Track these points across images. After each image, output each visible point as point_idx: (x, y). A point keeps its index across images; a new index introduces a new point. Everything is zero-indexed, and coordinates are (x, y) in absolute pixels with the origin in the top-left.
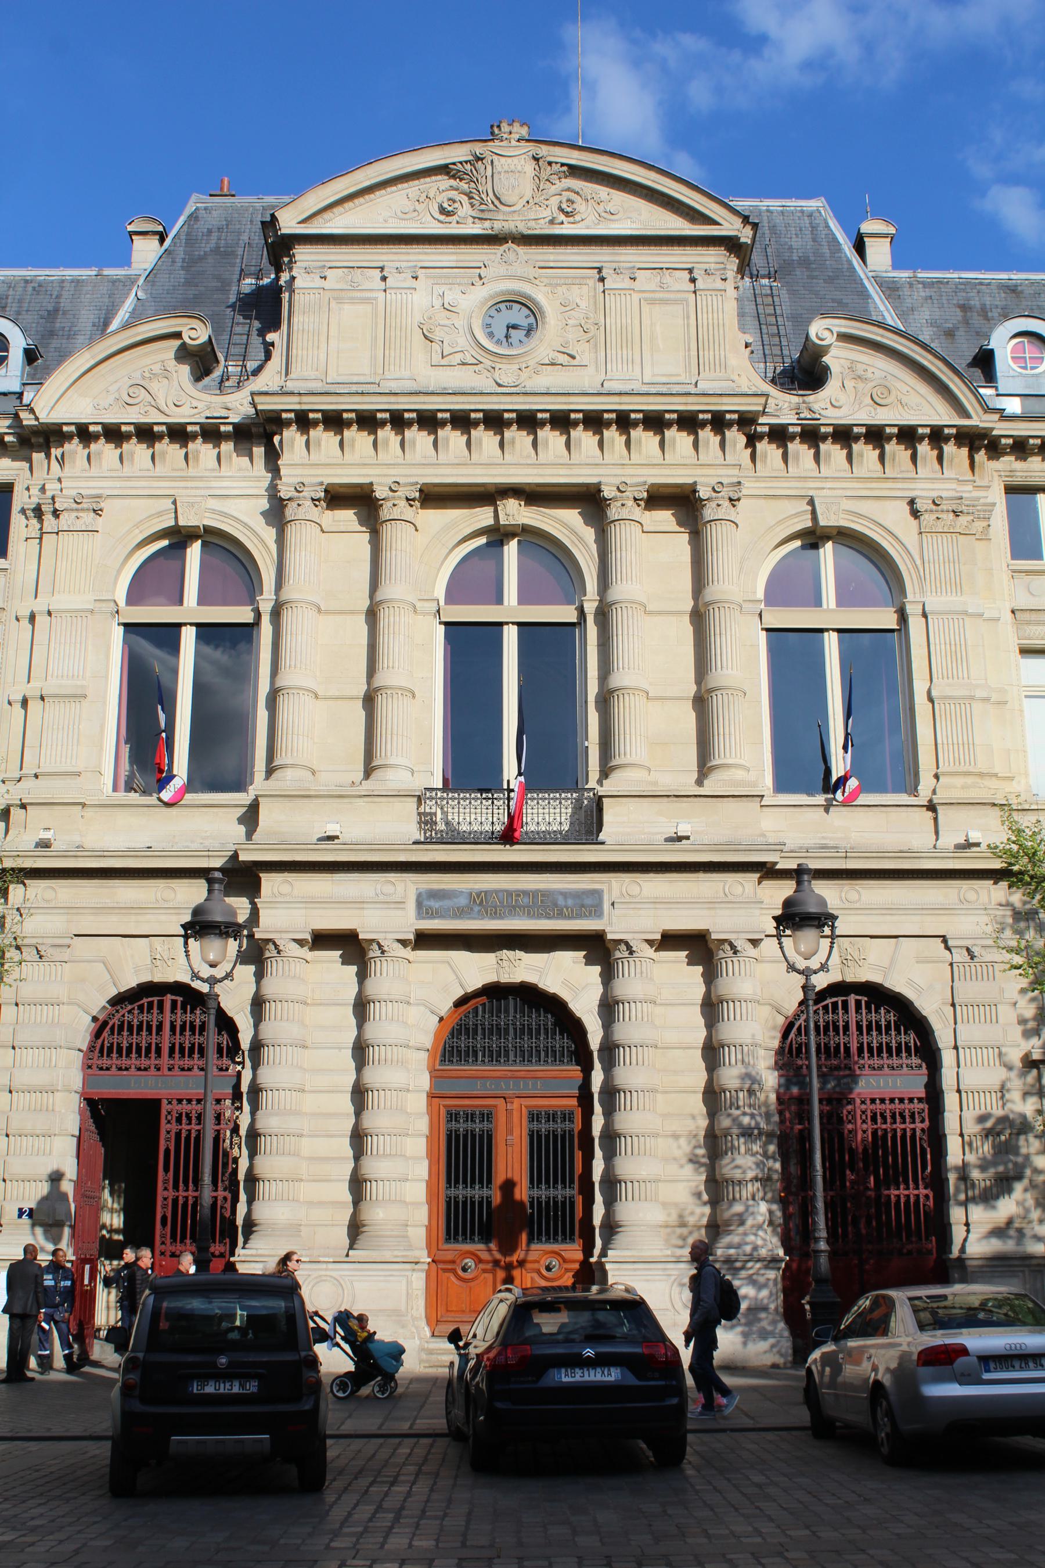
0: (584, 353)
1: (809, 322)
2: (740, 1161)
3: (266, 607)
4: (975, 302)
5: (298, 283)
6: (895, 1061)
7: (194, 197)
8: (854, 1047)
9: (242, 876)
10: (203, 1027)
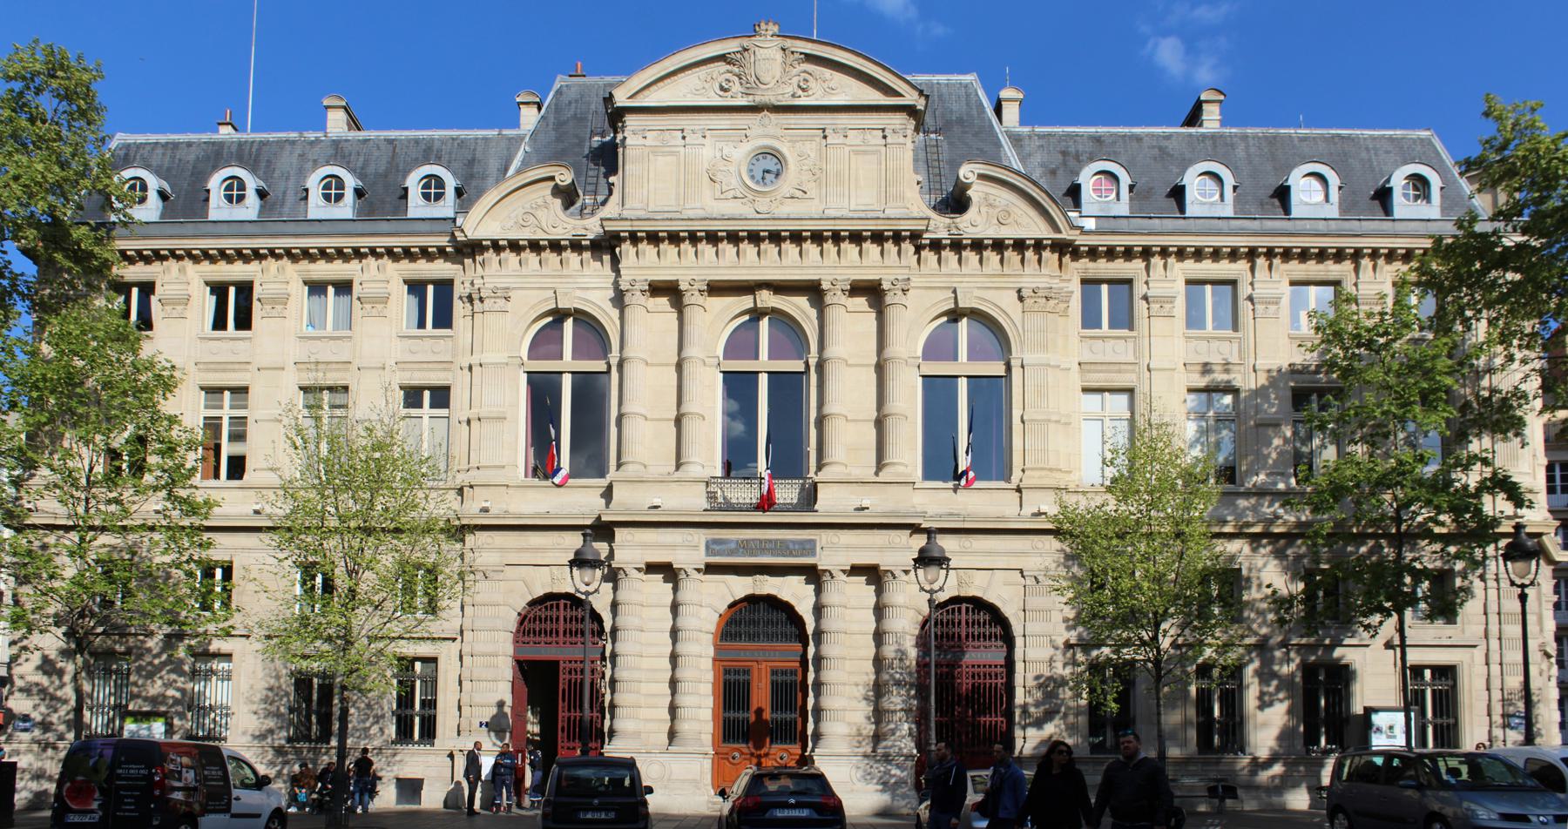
0: (811, 188)
1: (959, 165)
2: (893, 699)
3: (614, 362)
4: (1072, 149)
5: (628, 142)
6: (988, 643)
7: (559, 78)
8: (963, 635)
9: (603, 530)
10: (583, 619)
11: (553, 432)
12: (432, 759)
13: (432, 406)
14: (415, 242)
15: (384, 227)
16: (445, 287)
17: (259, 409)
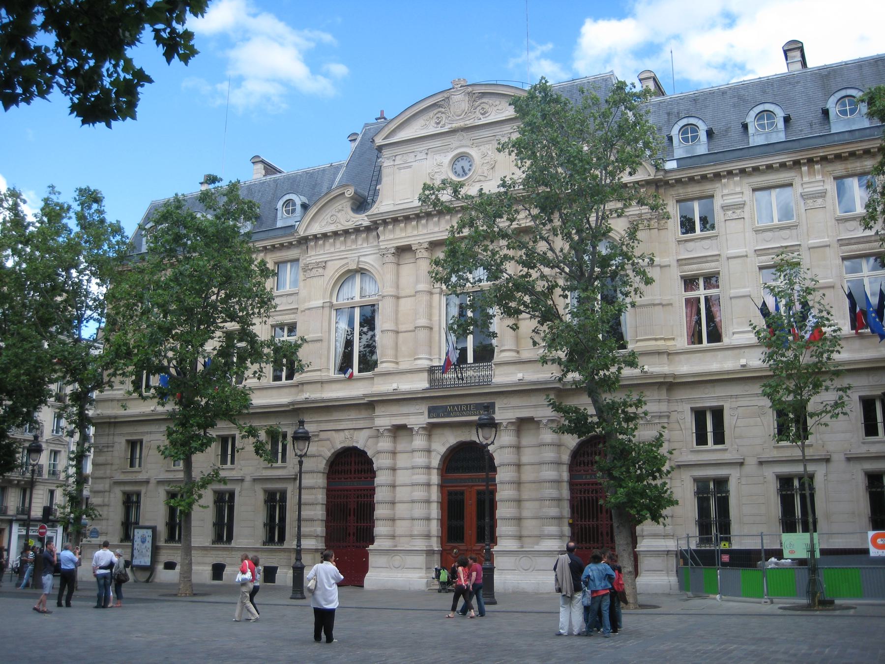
17: (727, 290)
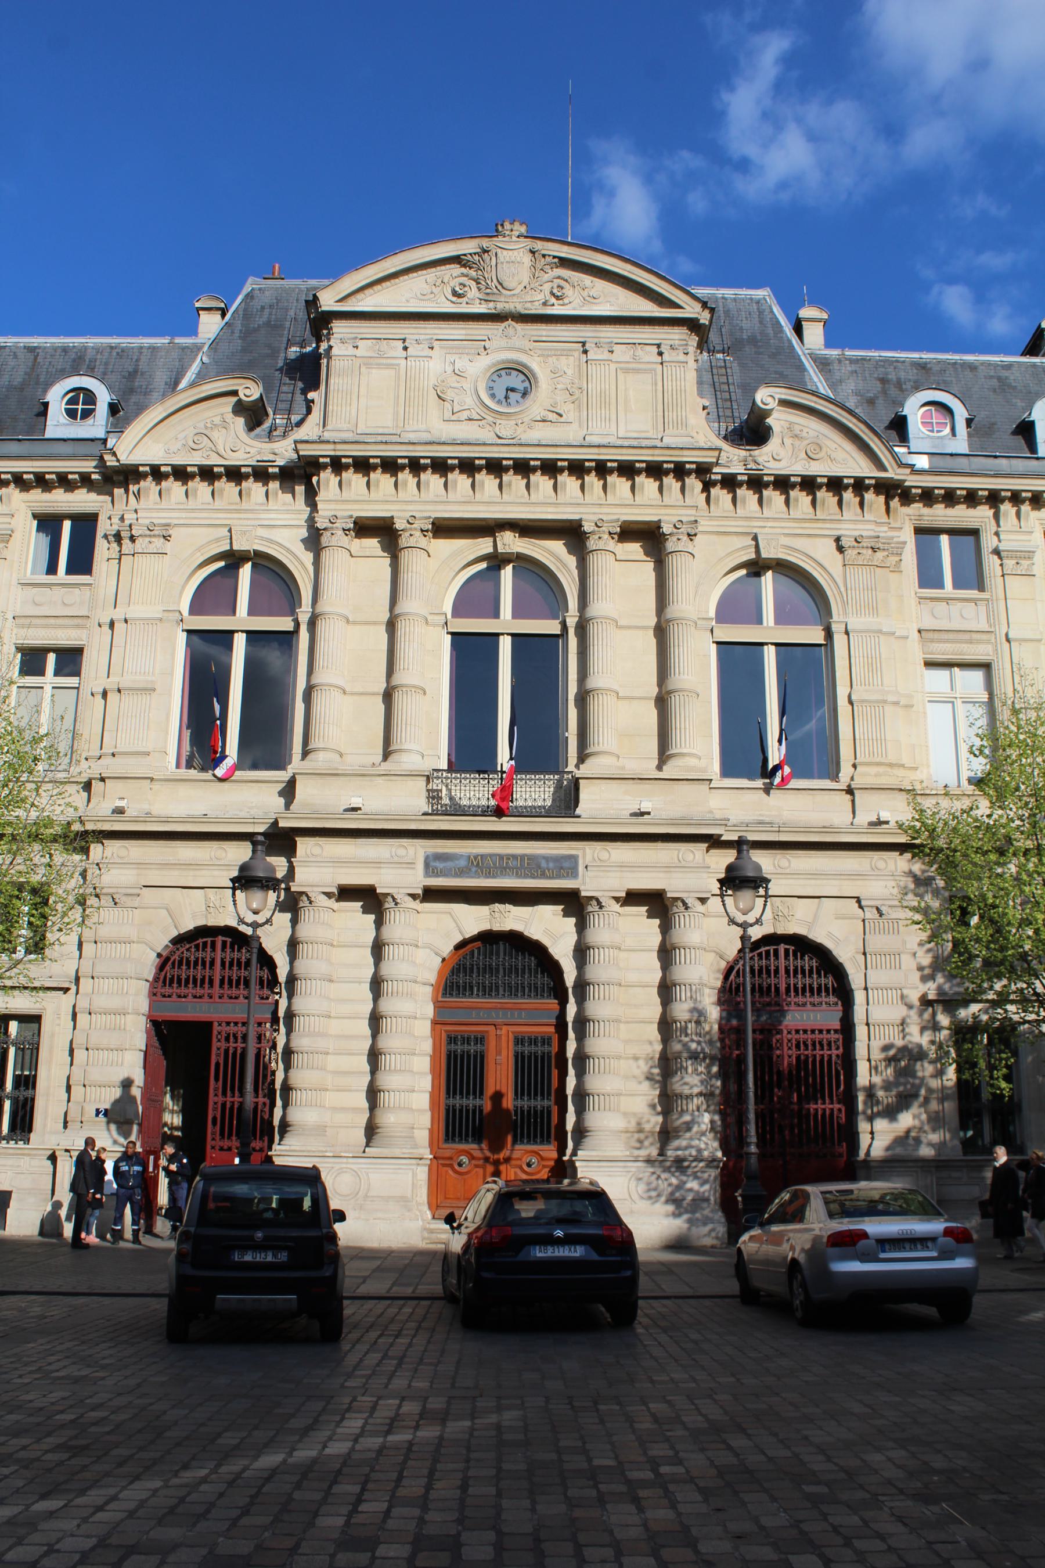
0: (569, 412)
1: (755, 390)
3: (304, 618)
4: (892, 376)
5: (335, 351)
6: (816, 999)
7: (251, 280)
8: (783, 987)
9: (281, 840)
10: (248, 963)
11: (217, 707)
12: (25, 1162)
13: (57, 673)
14: (51, 467)
15: (13, 448)
16: (85, 525)
